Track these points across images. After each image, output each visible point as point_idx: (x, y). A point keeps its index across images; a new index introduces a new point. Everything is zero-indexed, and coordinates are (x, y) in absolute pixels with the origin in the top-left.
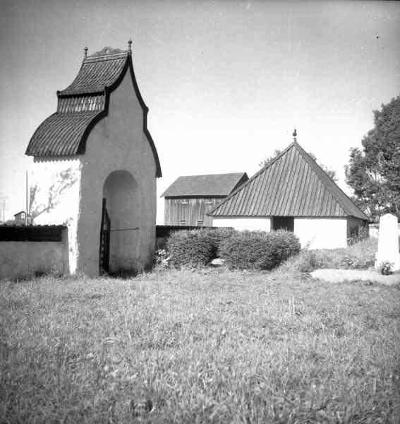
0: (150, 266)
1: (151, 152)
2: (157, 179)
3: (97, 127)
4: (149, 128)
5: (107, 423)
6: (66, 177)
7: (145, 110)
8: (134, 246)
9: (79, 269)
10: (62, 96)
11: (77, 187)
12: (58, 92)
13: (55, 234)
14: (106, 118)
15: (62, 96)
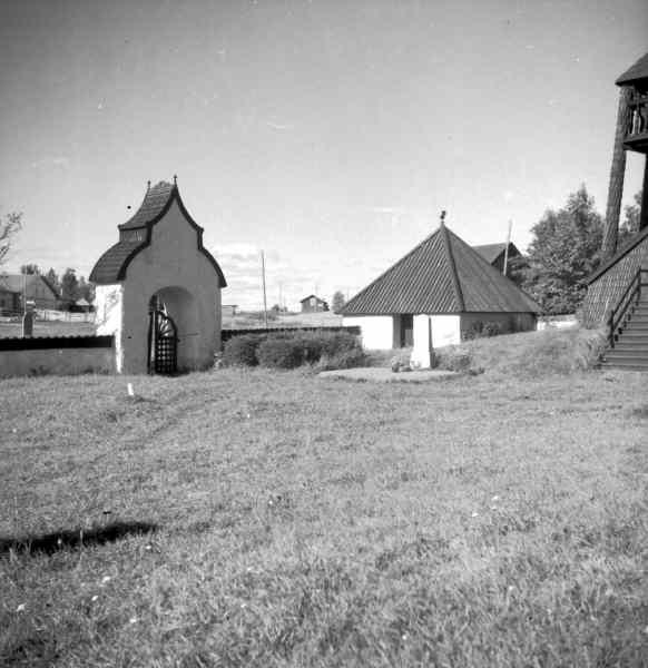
0: (208, 366)
1: (209, 263)
2: (222, 290)
3: (140, 256)
4: (205, 245)
5: (3, 439)
6: (113, 297)
7: (200, 231)
8: (192, 349)
9: (122, 369)
10: (122, 229)
11: (119, 306)
12: (119, 226)
13: (107, 342)
14: (149, 248)
15: (122, 229)
